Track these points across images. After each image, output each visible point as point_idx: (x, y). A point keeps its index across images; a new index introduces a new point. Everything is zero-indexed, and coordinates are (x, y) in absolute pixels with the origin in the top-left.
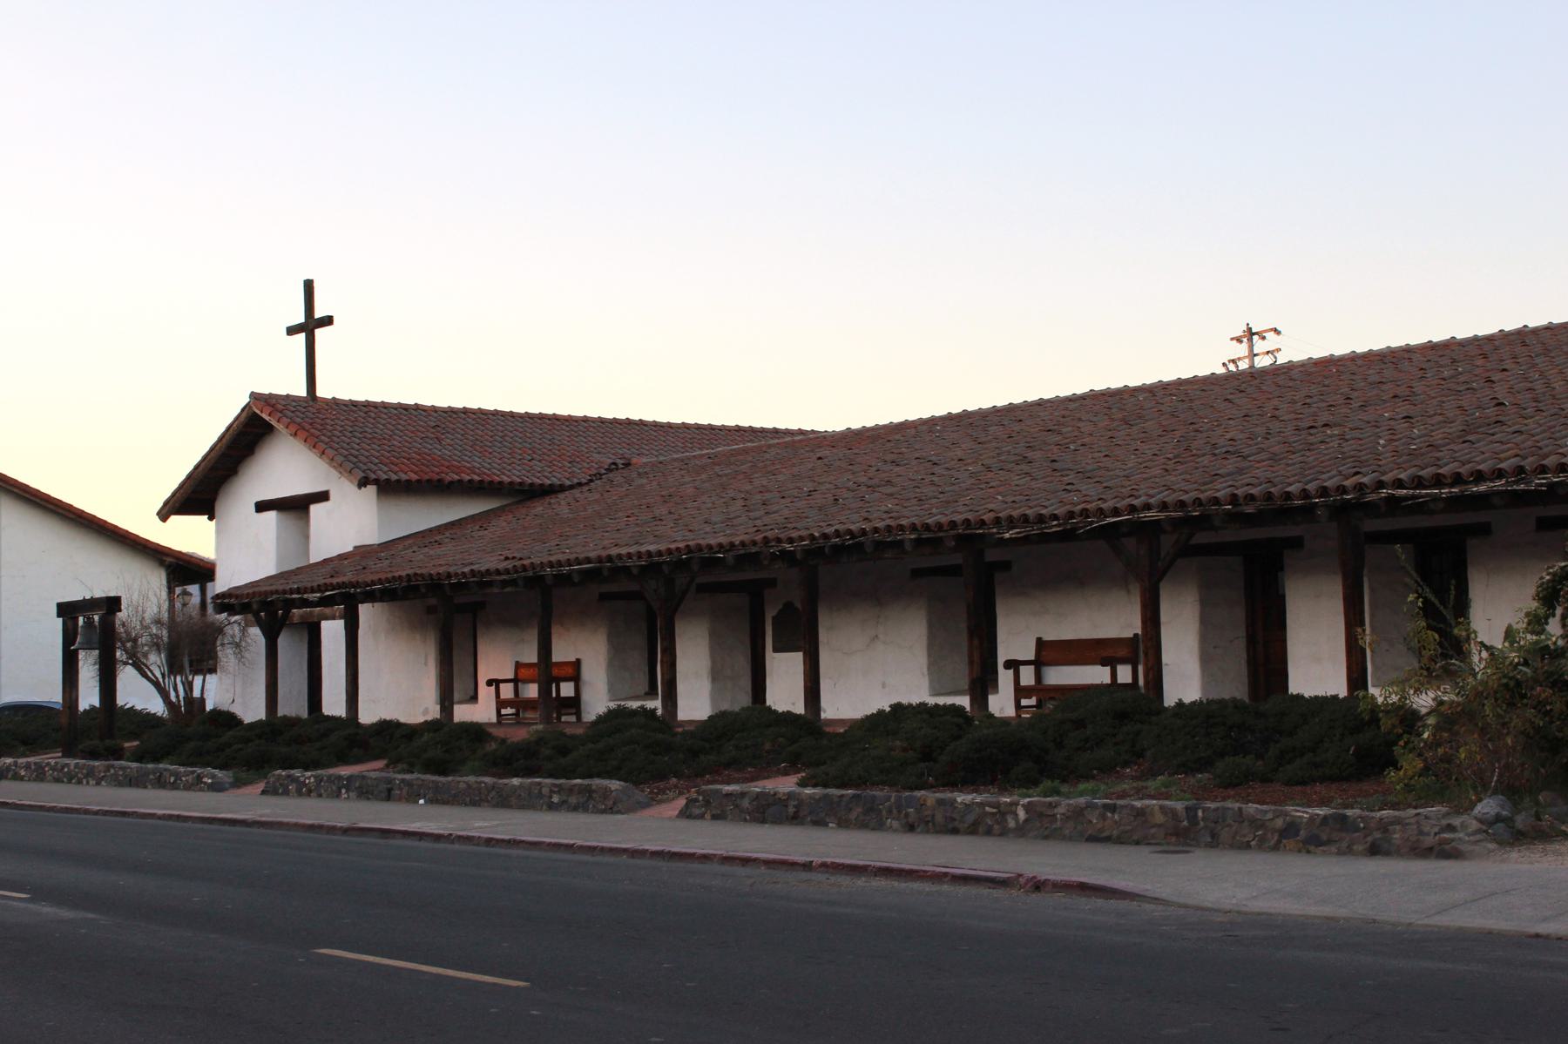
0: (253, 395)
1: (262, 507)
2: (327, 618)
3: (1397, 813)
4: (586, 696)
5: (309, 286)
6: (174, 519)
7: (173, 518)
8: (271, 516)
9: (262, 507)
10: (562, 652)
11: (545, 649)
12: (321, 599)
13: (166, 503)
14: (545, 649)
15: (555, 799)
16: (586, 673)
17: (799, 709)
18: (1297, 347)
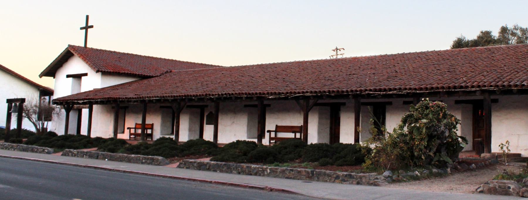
0: (70, 46)
1: (68, 76)
4: (154, 134)
5: (87, 17)
6: (44, 78)
8: (71, 79)
9: (68, 76)
10: (148, 121)
11: (144, 120)
13: (41, 73)
14: (144, 120)
16: (155, 127)
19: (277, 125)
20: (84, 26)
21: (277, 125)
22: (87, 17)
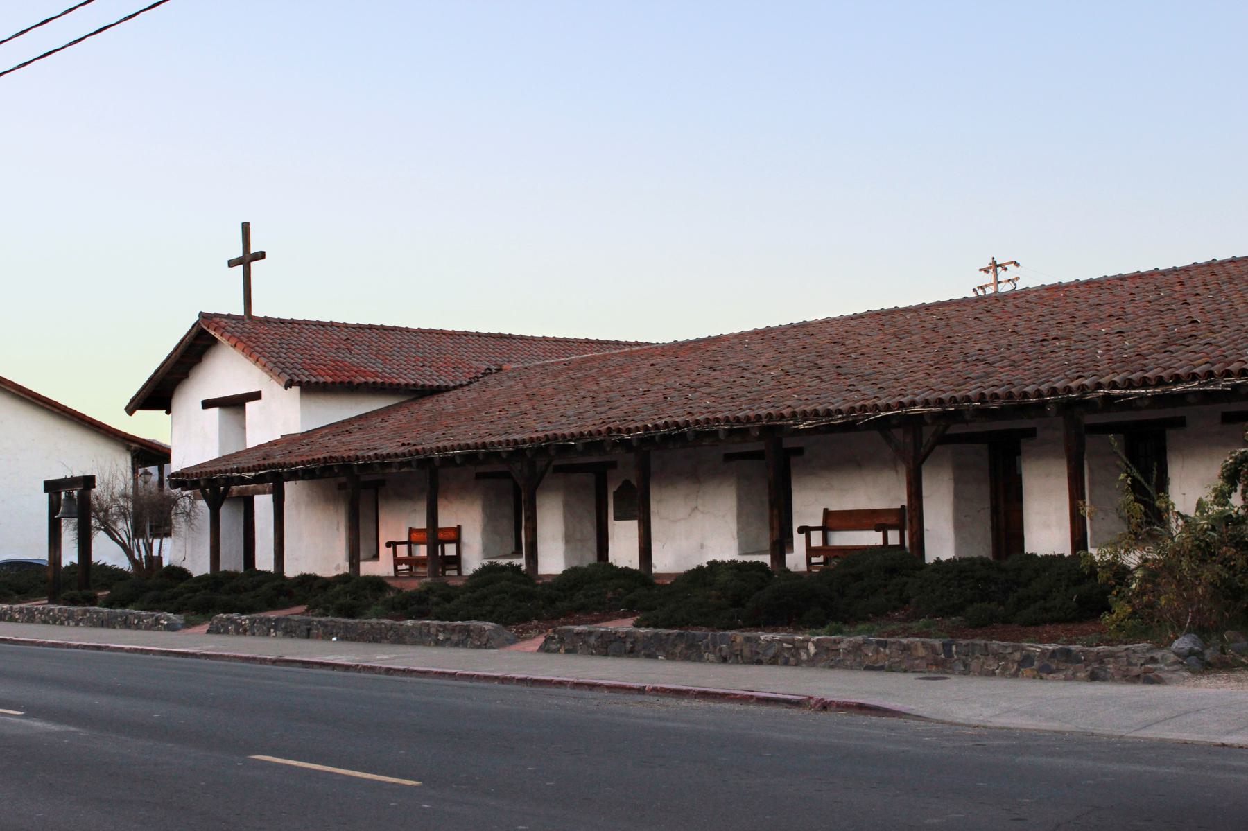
0: (202, 315)
1: (207, 404)
2: (259, 493)
3: (1111, 648)
4: (465, 555)
5: (246, 228)
6: (138, 413)
7: (138, 412)
8: (215, 411)
9: (207, 404)
11: (433, 517)
12: (254, 477)
13: (132, 401)
14: (433, 517)
15: (441, 637)
17: (635, 565)
18: (1031, 277)
19: (826, 511)
20: (239, 253)
21: (826, 511)
22: (246, 228)
